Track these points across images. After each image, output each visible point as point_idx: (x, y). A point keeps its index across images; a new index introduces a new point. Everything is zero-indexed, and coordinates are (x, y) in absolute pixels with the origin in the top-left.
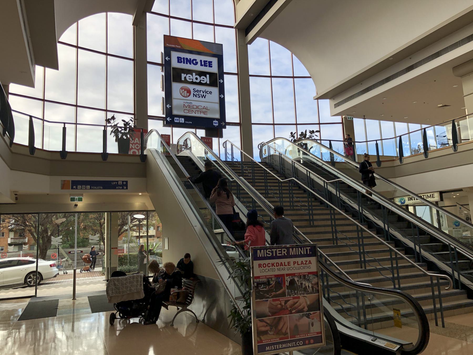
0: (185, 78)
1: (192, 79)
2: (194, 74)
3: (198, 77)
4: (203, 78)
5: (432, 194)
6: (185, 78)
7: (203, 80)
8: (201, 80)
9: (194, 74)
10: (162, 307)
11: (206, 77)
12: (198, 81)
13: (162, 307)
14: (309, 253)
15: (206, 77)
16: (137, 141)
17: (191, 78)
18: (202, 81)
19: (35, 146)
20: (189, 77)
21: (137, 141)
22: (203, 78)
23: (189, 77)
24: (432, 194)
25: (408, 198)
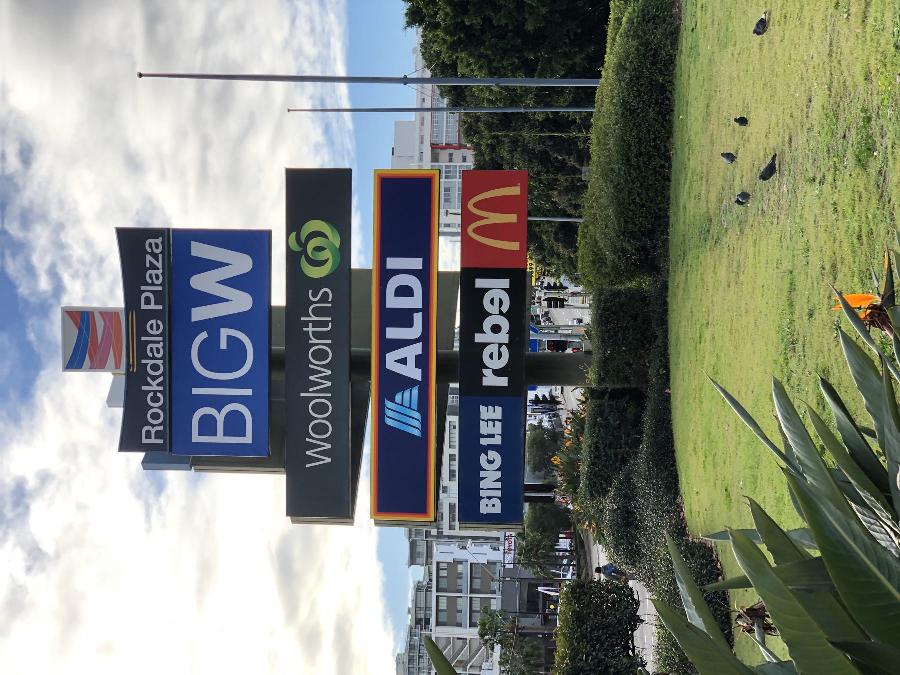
0: (497, 373)
1: (501, 345)
2: (479, 338)
3: (488, 324)
4: (492, 302)
5: (416, 530)
6: (497, 373)
7: (497, 302)
8: (501, 313)
9: (479, 338)
10: (481, 406)
11: (486, 290)
12: (505, 324)
13: (481, 406)
14: (330, 303)
15: (486, 290)
16: (404, 361)
17: (493, 349)
18: (505, 309)
19: (387, 368)
20: (491, 356)
21: (404, 361)
22: (492, 302)
23: (491, 356)
24: (416, 530)
25: (411, 530)
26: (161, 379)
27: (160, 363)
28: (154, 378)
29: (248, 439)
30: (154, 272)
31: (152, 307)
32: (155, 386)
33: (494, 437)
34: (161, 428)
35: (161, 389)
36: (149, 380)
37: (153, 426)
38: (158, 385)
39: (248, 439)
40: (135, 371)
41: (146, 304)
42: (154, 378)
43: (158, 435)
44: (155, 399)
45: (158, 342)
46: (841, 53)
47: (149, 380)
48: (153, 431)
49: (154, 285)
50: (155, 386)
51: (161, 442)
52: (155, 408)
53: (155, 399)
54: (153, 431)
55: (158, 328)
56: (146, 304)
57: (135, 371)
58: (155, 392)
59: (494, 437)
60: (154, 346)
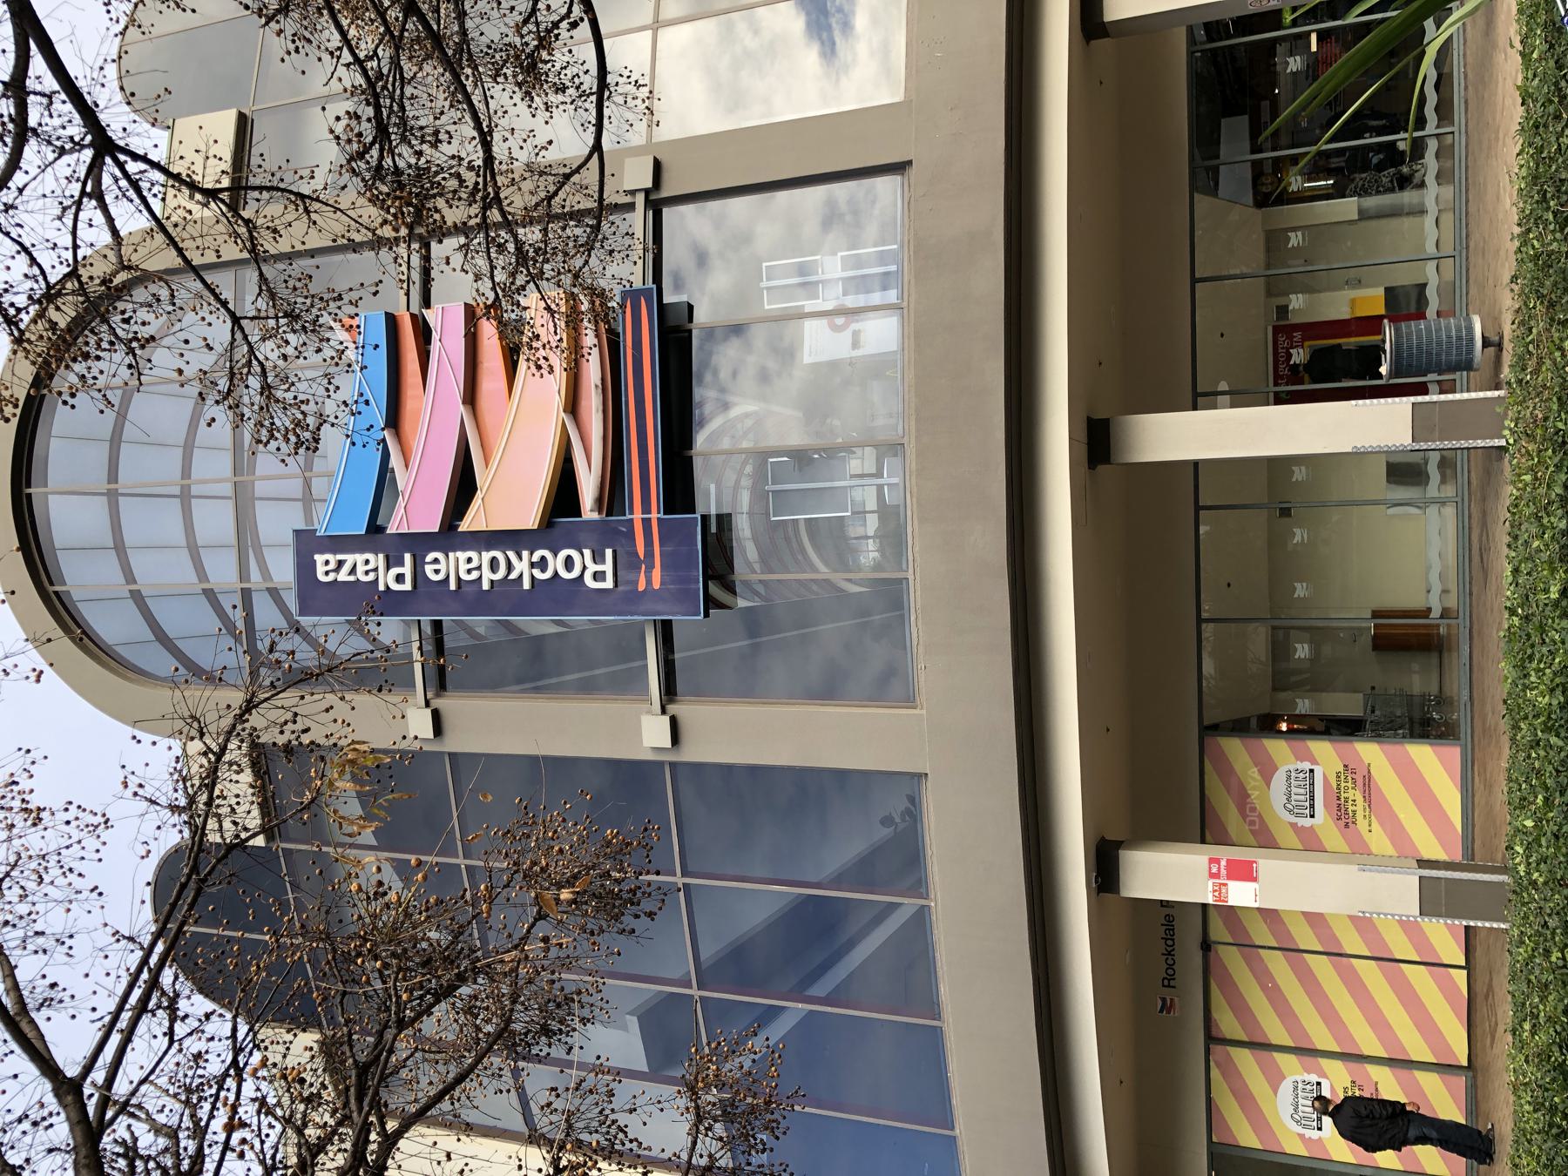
26: (511, 554)
27: (487, 556)
28: (510, 567)
29: (764, 264)
30: (361, 569)
31: (407, 570)
32: (521, 567)
33: (1373, 612)
34: (587, 553)
35: (525, 554)
36: (513, 576)
37: (585, 568)
38: (520, 558)
39: (764, 264)
40: (656, 585)
41: (604, 580)
42: (510, 567)
43: (598, 557)
44: (542, 564)
45: (457, 560)
46: (35, 921)
47: (513, 576)
48: (592, 568)
49: (376, 570)
50: (521, 567)
51: (609, 553)
52: (556, 564)
53: (542, 564)
54: (592, 568)
55: (436, 561)
56: (604, 580)
57: (656, 585)
58: (533, 565)
59: (1373, 612)
60: (463, 567)
